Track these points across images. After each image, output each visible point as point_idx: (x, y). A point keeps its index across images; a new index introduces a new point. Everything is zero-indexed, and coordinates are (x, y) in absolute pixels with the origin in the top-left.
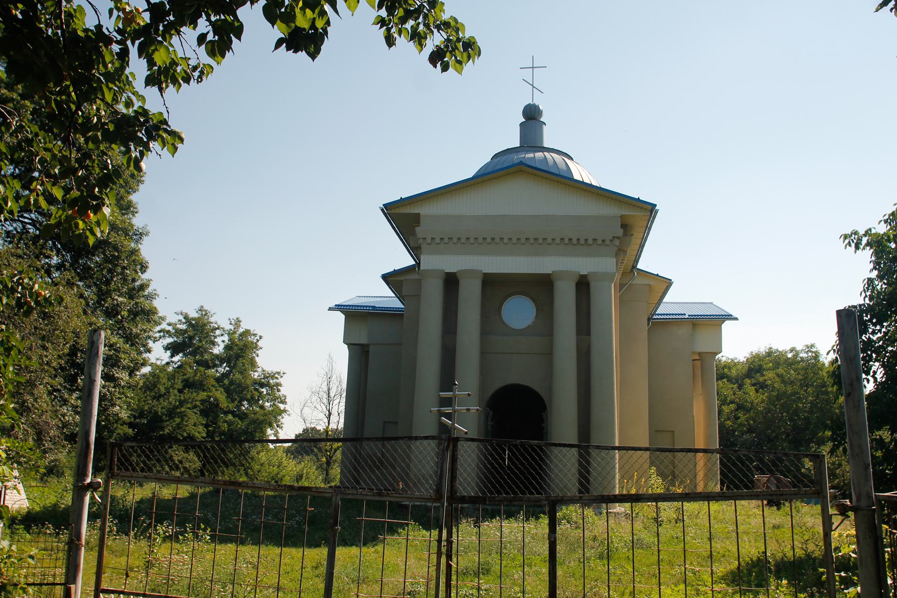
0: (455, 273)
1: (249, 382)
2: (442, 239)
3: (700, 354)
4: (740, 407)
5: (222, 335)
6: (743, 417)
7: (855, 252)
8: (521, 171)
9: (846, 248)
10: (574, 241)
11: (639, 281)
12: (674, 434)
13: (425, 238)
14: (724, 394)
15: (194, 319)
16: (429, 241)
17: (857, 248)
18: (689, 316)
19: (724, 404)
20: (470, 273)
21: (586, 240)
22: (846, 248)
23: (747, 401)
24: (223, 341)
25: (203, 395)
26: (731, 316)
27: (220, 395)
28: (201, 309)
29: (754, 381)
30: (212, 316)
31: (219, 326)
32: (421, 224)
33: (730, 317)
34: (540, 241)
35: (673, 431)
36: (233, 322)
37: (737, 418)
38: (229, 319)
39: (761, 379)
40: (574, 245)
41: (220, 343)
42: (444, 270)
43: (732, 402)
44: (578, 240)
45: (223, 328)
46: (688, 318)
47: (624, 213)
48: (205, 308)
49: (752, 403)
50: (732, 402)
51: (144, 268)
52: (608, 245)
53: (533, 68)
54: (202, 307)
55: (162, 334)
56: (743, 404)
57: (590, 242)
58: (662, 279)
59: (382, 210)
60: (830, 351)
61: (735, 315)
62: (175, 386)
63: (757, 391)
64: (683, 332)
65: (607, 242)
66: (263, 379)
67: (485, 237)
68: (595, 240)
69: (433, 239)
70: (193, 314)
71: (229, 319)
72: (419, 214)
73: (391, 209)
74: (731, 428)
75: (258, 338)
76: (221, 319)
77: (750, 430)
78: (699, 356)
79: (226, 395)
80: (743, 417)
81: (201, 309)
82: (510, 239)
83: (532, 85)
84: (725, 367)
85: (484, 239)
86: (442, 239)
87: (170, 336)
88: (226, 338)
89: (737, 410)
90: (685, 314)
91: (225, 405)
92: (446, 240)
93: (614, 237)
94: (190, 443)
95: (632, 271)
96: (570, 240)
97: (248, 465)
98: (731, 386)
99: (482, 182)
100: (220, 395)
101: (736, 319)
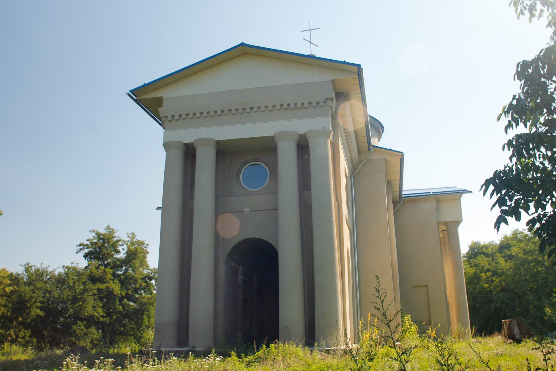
0: (192, 143)
1: (137, 276)
2: (180, 116)
3: (445, 223)
4: (495, 273)
5: (122, 245)
6: (497, 280)
7: (530, 21)
8: (246, 53)
9: (519, 18)
10: (292, 106)
11: (376, 156)
12: (428, 287)
13: (167, 117)
14: (482, 265)
15: (102, 235)
16: (170, 118)
17: (532, 15)
18: (433, 193)
19: (482, 273)
20: (205, 141)
21: (303, 104)
22: (519, 18)
23: (499, 269)
24: (123, 249)
25: (103, 286)
26: (467, 190)
27: (116, 287)
28: (108, 228)
29: (503, 255)
30: (116, 232)
31: (120, 239)
32: (163, 105)
33: (466, 191)
34: (263, 109)
35: (427, 286)
36: (130, 236)
37: (492, 281)
38: (127, 234)
39: (509, 253)
40: (292, 109)
41: (121, 250)
42: (182, 142)
43: (488, 270)
44: (296, 104)
45: (123, 240)
46: (432, 195)
47: (335, 78)
48: (111, 227)
49: (503, 269)
50: (488, 270)
51: (489, 336)
52: (322, 106)
53: (310, 30)
54: (109, 226)
55: (82, 247)
56: (496, 270)
57: (306, 105)
58: (395, 153)
59: (129, 95)
60: (501, 115)
61: (469, 190)
62: (80, 280)
63: (506, 261)
64: (430, 206)
65: (321, 104)
66: (151, 274)
67: (216, 110)
68: (310, 103)
69: (173, 116)
70: (103, 231)
71: (127, 234)
72: (162, 97)
73: (139, 96)
74: (488, 289)
75: (146, 245)
76: (121, 235)
77: (503, 290)
78: (446, 226)
79: (120, 285)
80: (497, 280)
81: (108, 228)
82: (237, 110)
83: (310, 42)
84: (483, 246)
85: (215, 112)
86: (180, 116)
87: (88, 248)
88: (125, 247)
89: (492, 276)
90: (430, 193)
91: (119, 292)
92: (184, 116)
93: (326, 99)
94: (91, 321)
95: (369, 149)
96: (289, 105)
97: (140, 335)
98: (487, 259)
99: (213, 66)
100: (116, 287)
101: (471, 192)
